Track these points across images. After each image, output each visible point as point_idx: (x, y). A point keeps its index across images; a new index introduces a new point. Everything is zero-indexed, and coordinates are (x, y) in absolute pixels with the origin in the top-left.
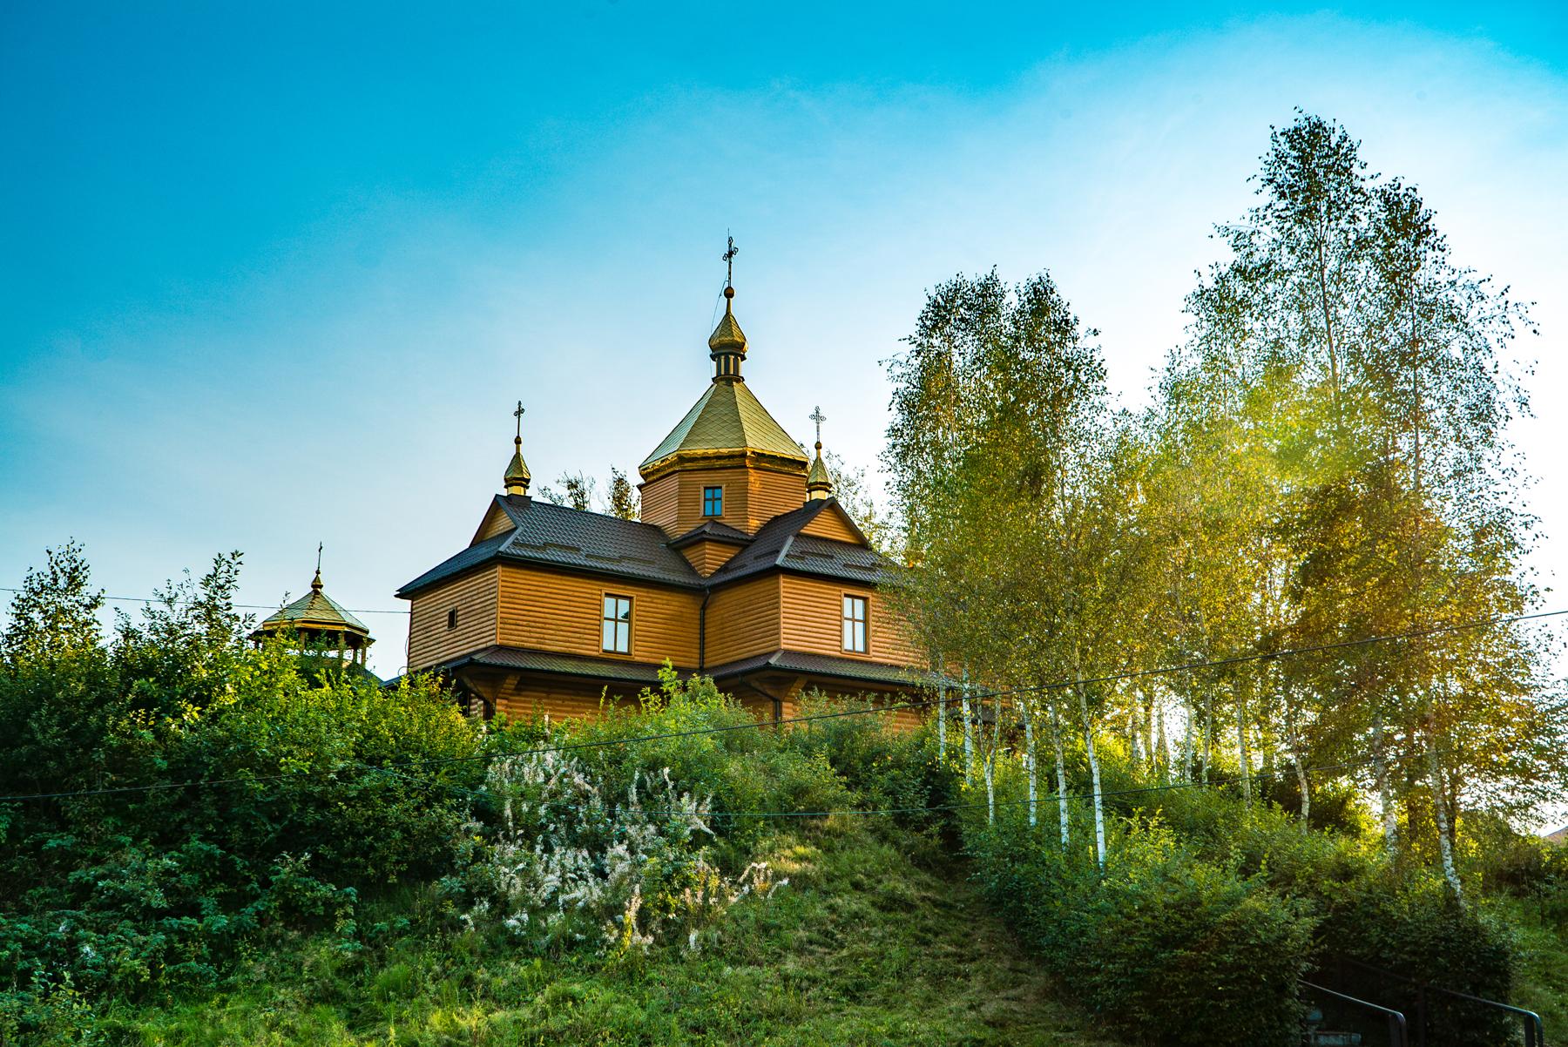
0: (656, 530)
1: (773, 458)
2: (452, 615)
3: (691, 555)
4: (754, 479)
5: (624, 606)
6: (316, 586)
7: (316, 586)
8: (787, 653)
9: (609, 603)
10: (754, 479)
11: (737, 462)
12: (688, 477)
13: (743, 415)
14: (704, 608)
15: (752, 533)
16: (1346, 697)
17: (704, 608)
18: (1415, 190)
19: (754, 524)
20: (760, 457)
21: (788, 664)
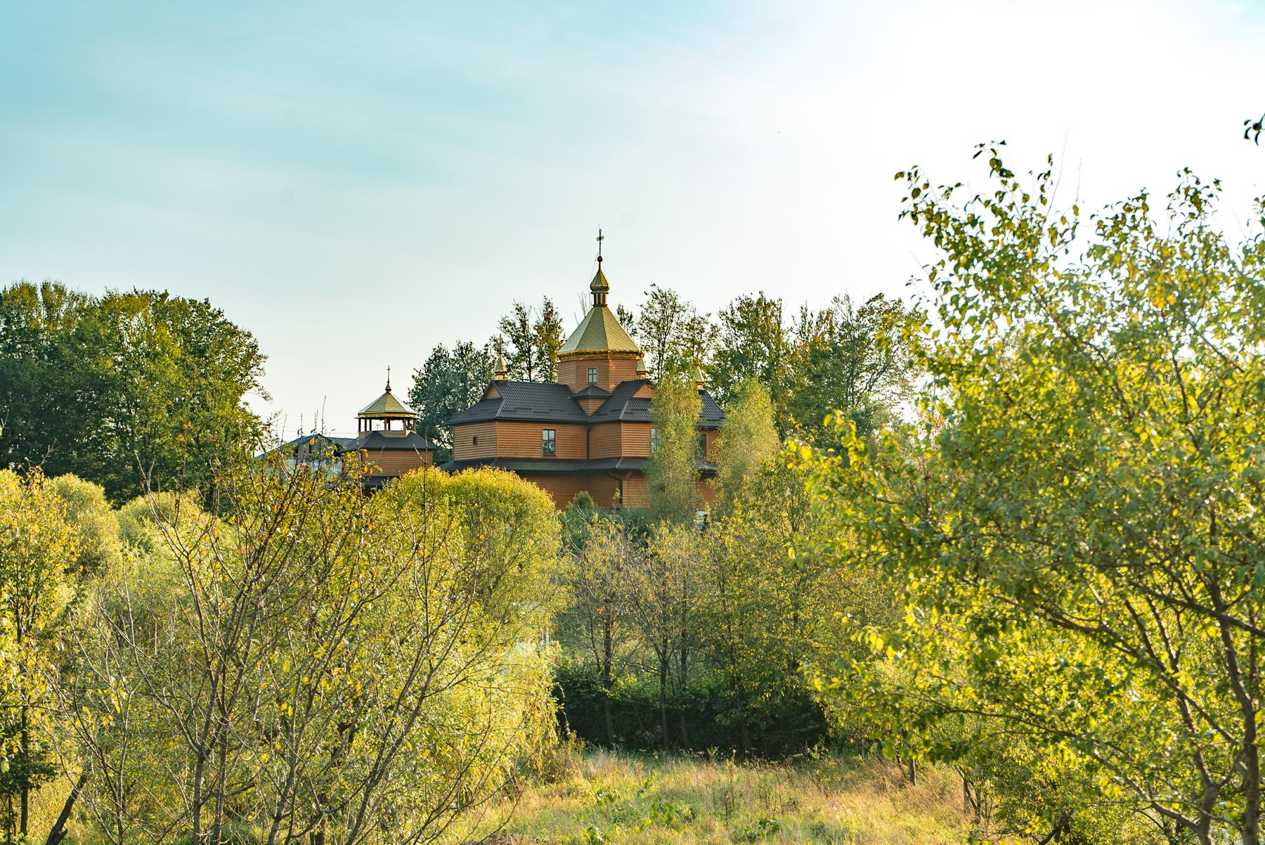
0: (566, 387)
1: (621, 352)
2: (475, 438)
3: (582, 403)
4: (612, 365)
5: (552, 433)
6: (388, 390)
7: (388, 390)
8: (626, 458)
9: (545, 433)
10: (612, 365)
11: (604, 356)
12: (580, 364)
13: (607, 329)
14: (588, 431)
15: (611, 391)
16: (533, 811)
17: (588, 431)
18: (880, 296)
19: (612, 386)
20: (614, 352)
21: (625, 467)
